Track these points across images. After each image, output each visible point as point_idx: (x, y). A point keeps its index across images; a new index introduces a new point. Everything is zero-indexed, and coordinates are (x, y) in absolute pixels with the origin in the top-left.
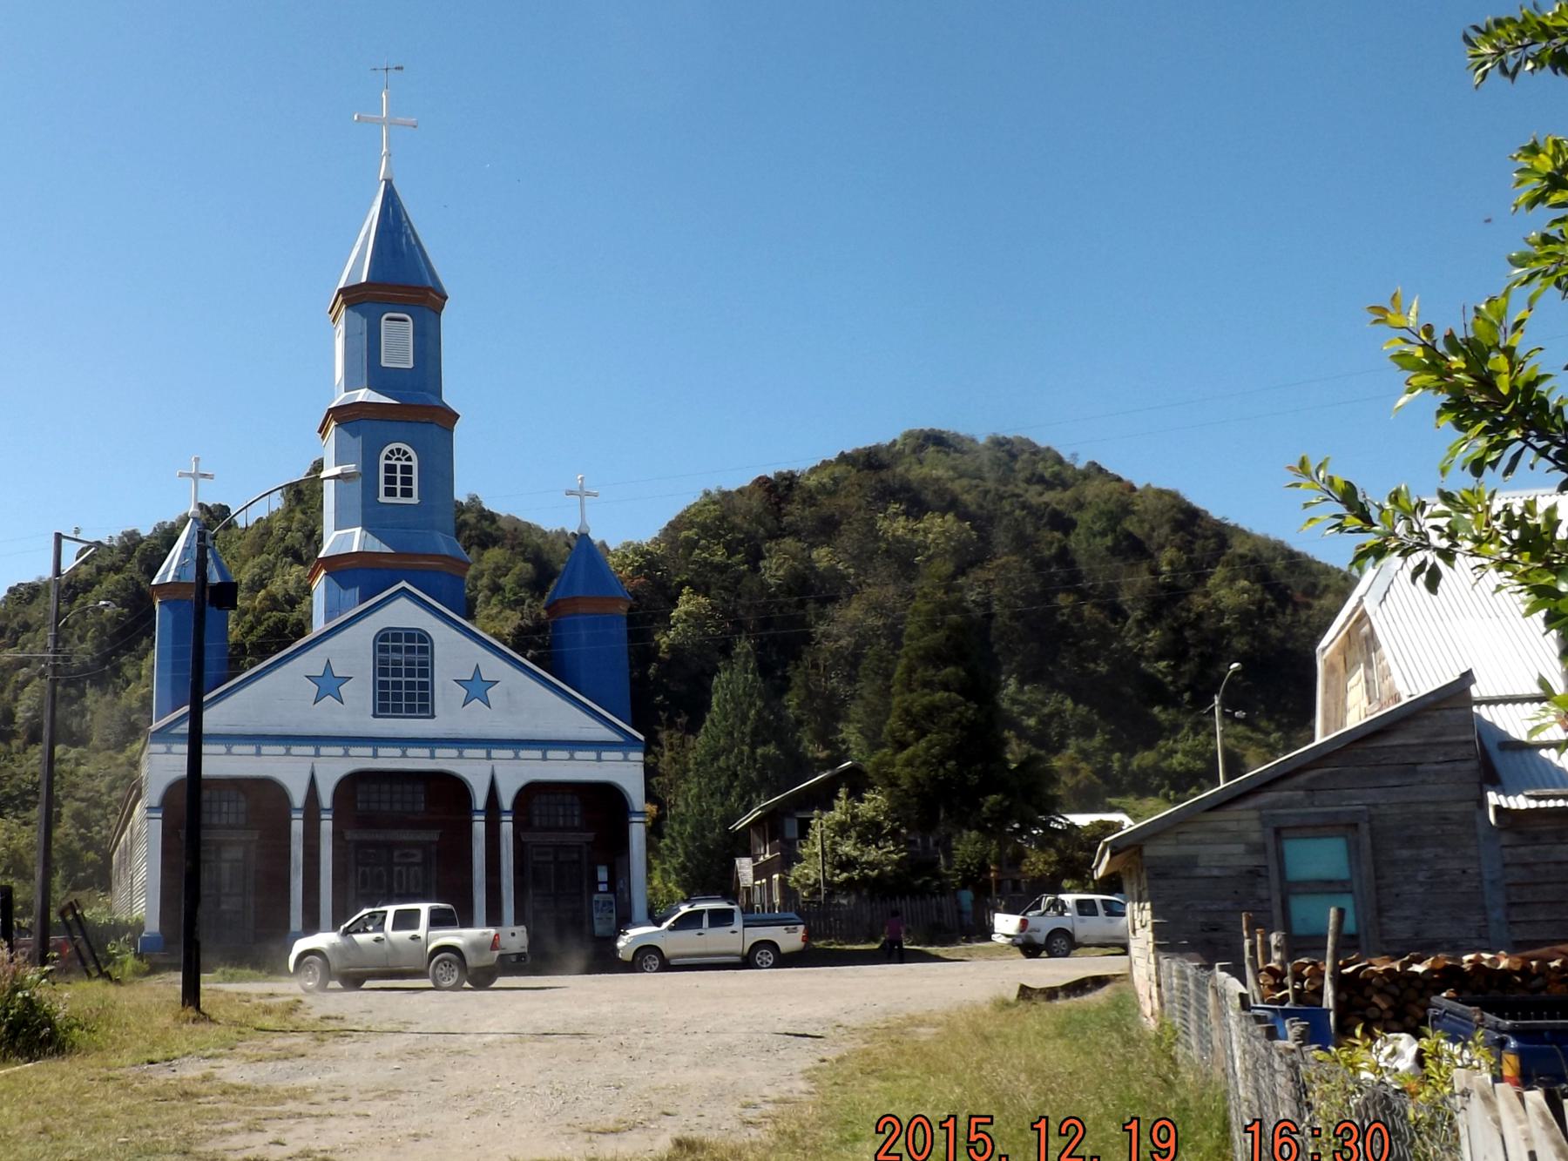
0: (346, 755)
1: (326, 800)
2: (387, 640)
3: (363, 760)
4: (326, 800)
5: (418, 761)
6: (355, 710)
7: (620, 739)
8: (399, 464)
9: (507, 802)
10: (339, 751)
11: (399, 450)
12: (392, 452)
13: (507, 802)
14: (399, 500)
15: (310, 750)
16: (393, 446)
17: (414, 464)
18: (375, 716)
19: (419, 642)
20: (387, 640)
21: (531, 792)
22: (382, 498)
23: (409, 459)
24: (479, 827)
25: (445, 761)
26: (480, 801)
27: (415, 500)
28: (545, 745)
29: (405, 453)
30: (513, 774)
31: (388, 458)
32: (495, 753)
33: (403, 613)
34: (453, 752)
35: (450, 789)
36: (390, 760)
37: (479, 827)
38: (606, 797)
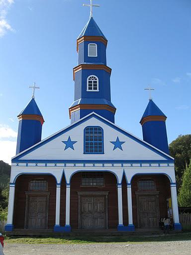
1: (68, 181)
2: (88, 130)
3: (80, 168)
4: (68, 181)
5: (99, 168)
6: (78, 152)
7: (165, 159)
9: (129, 181)
11: (93, 77)
12: (91, 78)
13: (129, 181)
14: (93, 90)
15: (63, 165)
16: (91, 76)
17: (98, 80)
18: (84, 153)
19: (99, 130)
20: (88, 130)
21: (137, 178)
22: (88, 90)
23: (96, 79)
24: (120, 190)
25: (108, 168)
27: (98, 90)
29: (95, 78)
30: (131, 172)
31: (89, 79)
32: (124, 165)
33: (94, 122)
35: (111, 177)
36: (89, 168)
37: (120, 190)
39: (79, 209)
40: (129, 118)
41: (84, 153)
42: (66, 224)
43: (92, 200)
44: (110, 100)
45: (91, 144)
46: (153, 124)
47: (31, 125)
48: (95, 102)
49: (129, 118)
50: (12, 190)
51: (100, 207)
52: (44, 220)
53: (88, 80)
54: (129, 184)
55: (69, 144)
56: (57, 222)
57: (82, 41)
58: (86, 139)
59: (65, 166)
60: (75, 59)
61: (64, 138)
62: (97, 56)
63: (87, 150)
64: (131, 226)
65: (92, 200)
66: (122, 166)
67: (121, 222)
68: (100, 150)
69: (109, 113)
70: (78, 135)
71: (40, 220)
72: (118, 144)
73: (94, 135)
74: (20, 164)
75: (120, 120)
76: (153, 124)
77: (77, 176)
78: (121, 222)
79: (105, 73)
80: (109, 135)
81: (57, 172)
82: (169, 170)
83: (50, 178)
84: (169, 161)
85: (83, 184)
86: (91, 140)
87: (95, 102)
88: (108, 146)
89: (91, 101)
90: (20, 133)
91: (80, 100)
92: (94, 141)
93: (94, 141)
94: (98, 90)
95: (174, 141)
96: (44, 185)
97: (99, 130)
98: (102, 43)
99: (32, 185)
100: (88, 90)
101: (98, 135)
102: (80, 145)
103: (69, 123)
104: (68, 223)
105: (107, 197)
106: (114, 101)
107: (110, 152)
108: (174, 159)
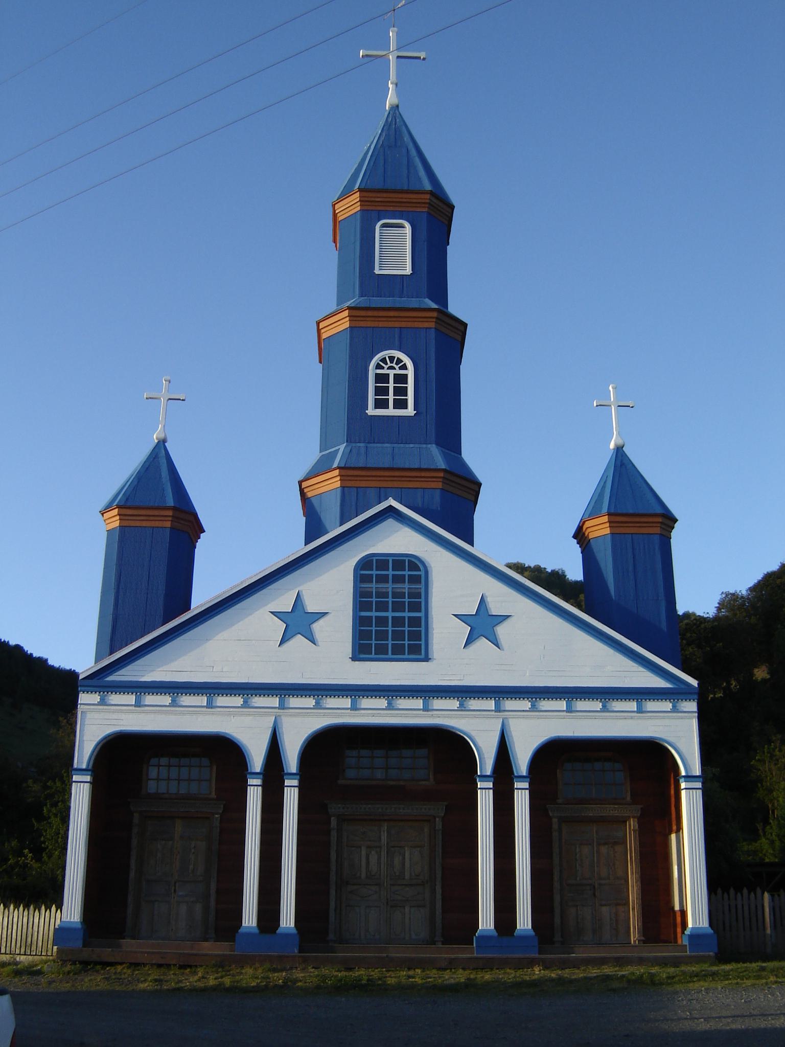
0: (318, 706)
2: (370, 570)
3: (339, 713)
5: (409, 714)
6: (330, 654)
7: (659, 683)
8: (391, 373)
9: (522, 760)
10: (310, 702)
12: (384, 360)
13: (522, 760)
14: (391, 411)
15: (274, 701)
17: (410, 373)
18: (354, 658)
19: (411, 570)
21: (553, 754)
22: (371, 411)
23: (404, 367)
25: (443, 714)
26: (486, 762)
28: (572, 693)
29: (399, 361)
31: (378, 367)
33: (396, 540)
34: (454, 704)
35: (451, 748)
36: (373, 713)
38: (652, 757)
39: (333, 867)
40: (534, 509)
41: (354, 658)
42: (243, 924)
43: (384, 837)
44: (459, 452)
45: (382, 621)
46: (620, 570)
47: (155, 553)
48: (405, 458)
49: (534, 509)
50: (81, 796)
51: (413, 860)
52: (198, 907)
53: (372, 372)
54: (521, 778)
55: (299, 623)
56: (250, 918)
57: (352, 206)
58: (362, 600)
59: (282, 706)
60: (317, 293)
61: (282, 598)
62: (408, 271)
63: (366, 645)
64: (524, 938)
65: (384, 837)
66: (498, 709)
67: (486, 920)
68: (412, 642)
69: (454, 502)
70: (332, 588)
71: (183, 908)
72: (482, 624)
73: (390, 587)
74: (115, 698)
75: (501, 528)
76: (620, 570)
77: (326, 746)
78: (486, 920)
79: (445, 343)
80: (453, 585)
81: (249, 730)
82: (679, 731)
83: (223, 752)
84: (676, 693)
85: (351, 773)
86: (382, 607)
87: (405, 458)
88: (444, 628)
89: (382, 454)
90: (115, 557)
91: (342, 447)
92: (391, 614)
93: (391, 614)
94: (410, 411)
95: (694, 614)
96: (198, 779)
97: (411, 570)
98: (434, 218)
99: (159, 777)
100: (371, 411)
101: (406, 587)
102: (337, 628)
103: (299, 548)
104: (288, 919)
105: (439, 825)
106: (475, 453)
107: (451, 657)
108: (694, 683)
